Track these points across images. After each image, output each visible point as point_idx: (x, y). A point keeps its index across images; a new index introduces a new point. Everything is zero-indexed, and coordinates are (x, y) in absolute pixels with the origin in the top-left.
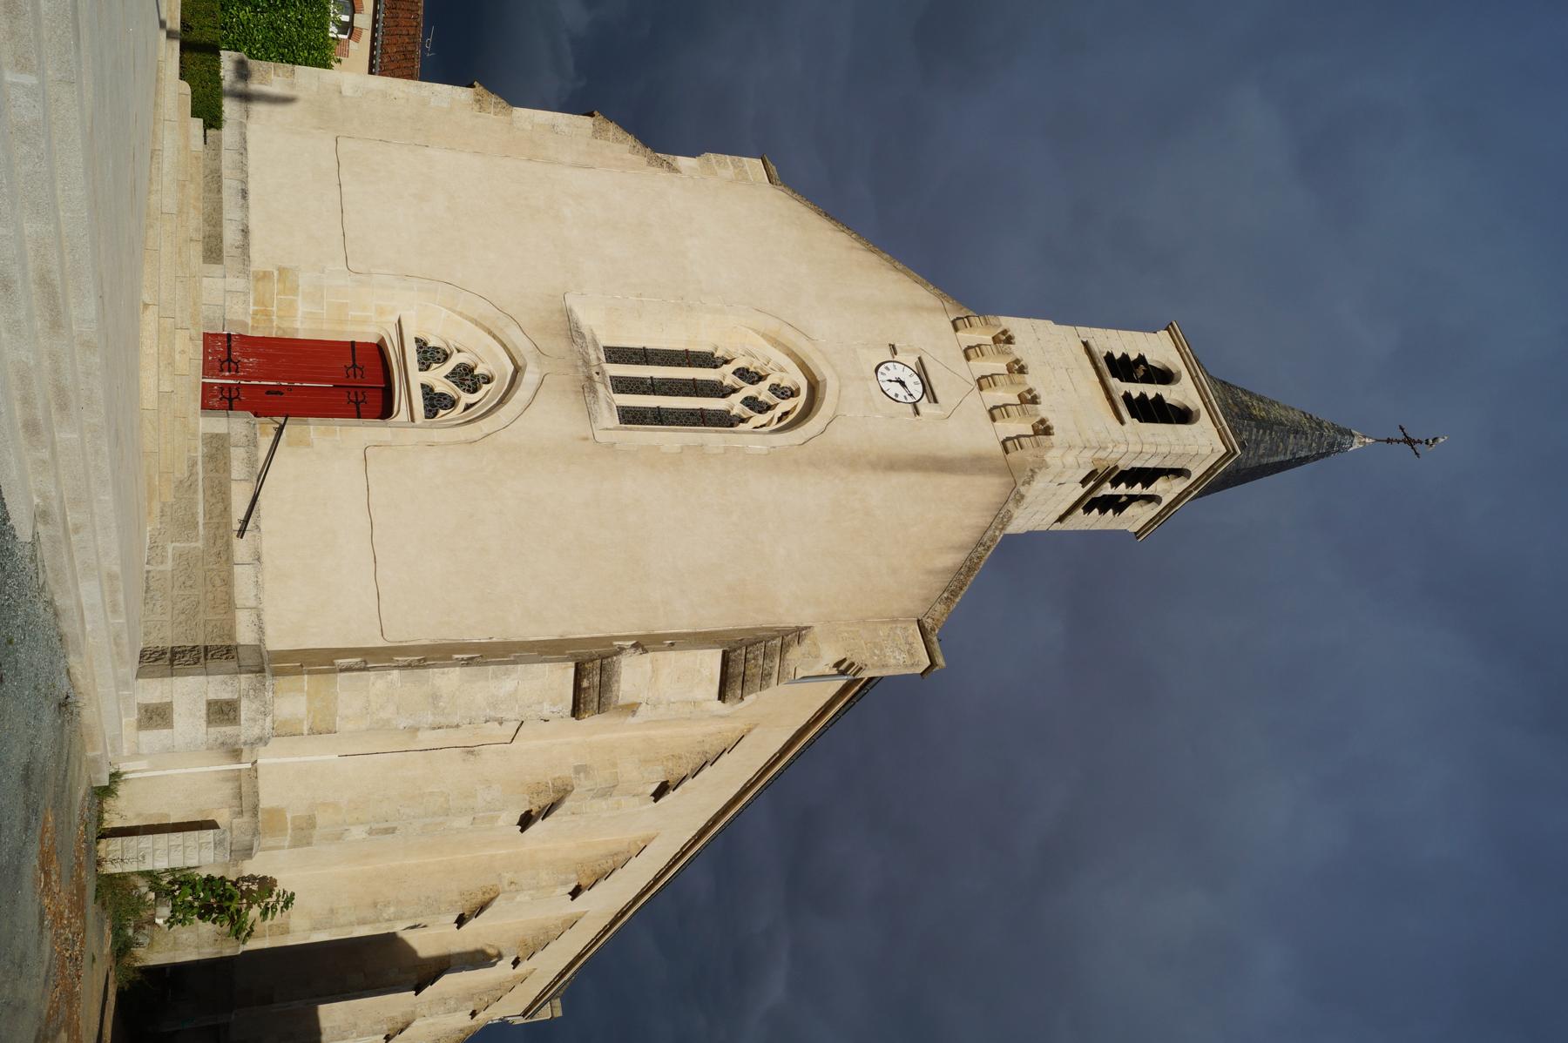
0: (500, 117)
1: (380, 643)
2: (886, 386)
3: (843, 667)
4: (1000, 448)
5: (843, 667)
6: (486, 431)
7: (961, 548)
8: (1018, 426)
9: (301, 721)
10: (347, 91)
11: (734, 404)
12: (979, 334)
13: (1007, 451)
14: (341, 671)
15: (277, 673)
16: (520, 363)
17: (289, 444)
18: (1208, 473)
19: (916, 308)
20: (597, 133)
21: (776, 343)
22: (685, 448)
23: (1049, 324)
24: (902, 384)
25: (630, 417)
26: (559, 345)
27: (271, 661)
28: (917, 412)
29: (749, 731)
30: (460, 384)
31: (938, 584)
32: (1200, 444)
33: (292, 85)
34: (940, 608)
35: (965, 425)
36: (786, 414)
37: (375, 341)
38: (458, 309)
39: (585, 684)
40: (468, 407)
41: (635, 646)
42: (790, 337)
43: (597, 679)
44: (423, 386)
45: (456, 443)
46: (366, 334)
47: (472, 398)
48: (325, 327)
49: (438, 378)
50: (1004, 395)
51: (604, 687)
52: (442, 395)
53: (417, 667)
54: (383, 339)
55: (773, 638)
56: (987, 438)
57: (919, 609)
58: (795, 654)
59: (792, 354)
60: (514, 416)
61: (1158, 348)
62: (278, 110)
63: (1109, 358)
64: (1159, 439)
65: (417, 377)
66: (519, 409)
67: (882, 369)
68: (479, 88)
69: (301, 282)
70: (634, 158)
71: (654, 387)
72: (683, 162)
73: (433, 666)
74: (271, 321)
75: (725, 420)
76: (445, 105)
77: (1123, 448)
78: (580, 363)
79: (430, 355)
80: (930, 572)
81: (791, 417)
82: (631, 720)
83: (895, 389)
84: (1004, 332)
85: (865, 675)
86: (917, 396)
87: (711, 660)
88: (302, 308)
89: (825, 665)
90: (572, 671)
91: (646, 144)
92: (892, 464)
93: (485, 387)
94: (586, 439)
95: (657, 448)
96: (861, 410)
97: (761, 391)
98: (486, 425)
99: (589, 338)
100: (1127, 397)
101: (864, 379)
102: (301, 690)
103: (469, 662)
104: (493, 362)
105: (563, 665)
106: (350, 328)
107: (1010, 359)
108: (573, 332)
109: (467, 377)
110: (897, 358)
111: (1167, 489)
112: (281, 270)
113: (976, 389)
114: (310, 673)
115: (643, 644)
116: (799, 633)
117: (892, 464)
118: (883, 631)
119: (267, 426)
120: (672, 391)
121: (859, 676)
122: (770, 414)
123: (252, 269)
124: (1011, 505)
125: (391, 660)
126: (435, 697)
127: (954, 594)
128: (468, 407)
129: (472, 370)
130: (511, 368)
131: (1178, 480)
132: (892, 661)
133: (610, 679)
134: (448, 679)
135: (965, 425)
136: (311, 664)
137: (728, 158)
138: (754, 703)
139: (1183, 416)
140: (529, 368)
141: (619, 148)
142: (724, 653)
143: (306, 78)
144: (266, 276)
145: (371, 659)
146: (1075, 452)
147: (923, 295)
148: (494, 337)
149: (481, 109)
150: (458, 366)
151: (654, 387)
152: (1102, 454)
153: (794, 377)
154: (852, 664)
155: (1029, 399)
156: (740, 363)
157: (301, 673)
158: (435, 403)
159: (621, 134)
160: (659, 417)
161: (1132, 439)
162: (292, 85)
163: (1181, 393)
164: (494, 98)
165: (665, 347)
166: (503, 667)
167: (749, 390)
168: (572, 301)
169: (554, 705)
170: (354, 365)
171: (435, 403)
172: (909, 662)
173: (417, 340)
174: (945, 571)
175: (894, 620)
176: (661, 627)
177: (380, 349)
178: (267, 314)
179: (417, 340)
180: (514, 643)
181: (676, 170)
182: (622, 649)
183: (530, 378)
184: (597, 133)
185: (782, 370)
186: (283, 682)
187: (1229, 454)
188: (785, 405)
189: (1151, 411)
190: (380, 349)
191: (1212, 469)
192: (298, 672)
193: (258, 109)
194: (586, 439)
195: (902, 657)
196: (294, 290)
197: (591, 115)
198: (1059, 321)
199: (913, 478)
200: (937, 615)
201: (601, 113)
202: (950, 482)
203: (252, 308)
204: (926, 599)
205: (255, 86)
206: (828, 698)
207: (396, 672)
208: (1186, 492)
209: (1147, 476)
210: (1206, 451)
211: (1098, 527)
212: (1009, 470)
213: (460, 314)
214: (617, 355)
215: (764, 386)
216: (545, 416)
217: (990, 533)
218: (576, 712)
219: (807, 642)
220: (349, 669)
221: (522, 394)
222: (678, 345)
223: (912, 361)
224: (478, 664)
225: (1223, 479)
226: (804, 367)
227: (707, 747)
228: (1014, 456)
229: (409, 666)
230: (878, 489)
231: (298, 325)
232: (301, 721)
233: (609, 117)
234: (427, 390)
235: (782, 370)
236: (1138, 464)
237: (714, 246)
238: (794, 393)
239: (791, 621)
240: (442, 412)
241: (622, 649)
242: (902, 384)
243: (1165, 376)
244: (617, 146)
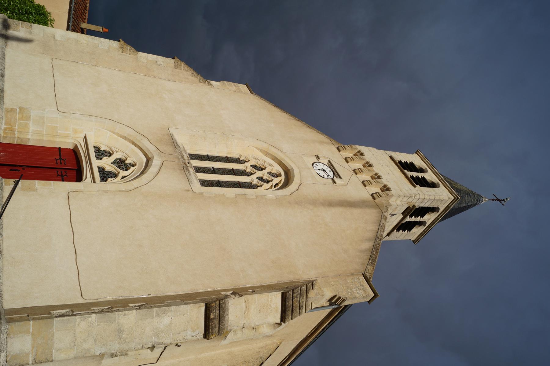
0: (132, 56)
1: (80, 301)
2: (319, 172)
3: (333, 301)
4: (371, 197)
5: (333, 301)
6: (136, 186)
7: (369, 240)
8: (375, 189)
9: (28, 354)
10: (58, 37)
11: (253, 180)
12: (348, 153)
13: (374, 198)
14: (56, 317)
15: (9, 321)
16: (150, 156)
17: (22, 190)
18: (445, 209)
19: (321, 143)
20: (176, 66)
21: (267, 154)
22: (237, 195)
23: (374, 149)
24: (324, 170)
25: (205, 183)
26: (169, 149)
27: (6, 314)
28: (334, 182)
29: (281, 343)
30: (119, 167)
31: (365, 257)
32: (442, 196)
33: (30, 33)
34: (370, 268)
35: (353, 188)
36: (277, 184)
37: (71, 147)
38: (116, 131)
39: (212, 316)
40: (123, 177)
41: (232, 294)
42: (273, 151)
43: (217, 313)
44: (99, 167)
45: (120, 191)
46: (67, 143)
47: (125, 173)
48: (44, 138)
49: (107, 163)
50: (365, 176)
51: (221, 318)
52: (109, 172)
53: (108, 312)
54: (76, 146)
55: (303, 286)
56: (365, 193)
57: (362, 270)
58: (312, 294)
59: (275, 159)
60: (149, 179)
61: (417, 161)
62: (22, 46)
63: (400, 162)
64: (430, 193)
65: (96, 163)
66: (152, 176)
67: (314, 165)
68: (122, 42)
69: (32, 114)
70: (193, 78)
71: (215, 171)
72: (213, 83)
73: (118, 310)
74: (14, 134)
75: (249, 186)
76: (106, 48)
77: (418, 197)
78: (180, 157)
79: (101, 154)
80: (361, 251)
81: (280, 185)
82: (224, 342)
83: (322, 173)
84: (359, 152)
85: (344, 304)
86: (332, 176)
87: (276, 298)
88: (32, 128)
89: (324, 302)
90: (203, 309)
91: (198, 73)
92: (330, 204)
93: (132, 168)
94: (188, 191)
95: (224, 195)
96: (310, 179)
97: (264, 174)
98: (136, 183)
99: (182, 148)
100: (412, 177)
101: (308, 168)
102: (28, 332)
103: (140, 307)
104: (135, 156)
105: (198, 305)
106: (58, 140)
107: (364, 162)
108: (175, 144)
109: (121, 164)
110: (320, 161)
111: (429, 218)
112: (21, 109)
113: (354, 174)
114: (33, 319)
115: (238, 292)
116: (311, 284)
117: (330, 204)
118: (349, 280)
119: (12, 182)
120: (222, 173)
121: (341, 305)
122: (270, 184)
123: (4, 107)
124: (383, 221)
125: (89, 309)
126: (120, 331)
127: (374, 261)
128: (123, 177)
129: (124, 161)
130: (145, 160)
131: (433, 214)
132: (357, 295)
133: (224, 313)
134: (128, 319)
135: (353, 188)
136: (35, 314)
137: (232, 83)
138: (291, 323)
139: (433, 185)
140: (155, 158)
141: (186, 74)
142: (283, 294)
143: (37, 30)
144: (12, 110)
145: (74, 310)
146: (400, 199)
147: (322, 137)
148: (136, 145)
149: (123, 51)
150: (117, 159)
151: (215, 171)
152: (410, 200)
153: (277, 169)
154: (340, 298)
155: (377, 177)
156: (253, 162)
157: (29, 320)
158: (105, 175)
159: (187, 67)
160: (219, 184)
161: (420, 193)
162: (30, 33)
163: (430, 176)
164: (129, 47)
165: (203, 174)
166: (162, 309)
167: (259, 174)
168: (172, 131)
169: (193, 331)
170: (60, 159)
171: (105, 175)
172: (365, 295)
173: (94, 147)
174: (367, 250)
175: (352, 274)
176: (243, 284)
177: (75, 152)
178: (13, 131)
179: (94, 147)
180: (163, 297)
181: (211, 85)
182: (227, 296)
183: (156, 162)
184: (176, 66)
185: (271, 165)
186: (14, 327)
187: (455, 199)
188: (276, 180)
189: (423, 183)
190: (75, 152)
191: (448, 207)
192: (27, 319)
193: (12, 44)
194: (188, 191)
195: (361, 293)
196: (28, 118)
197: (174, 58)
198: (378, 148)
199: (341, 209)
200: (370, 271)
201: (178, 58)
202: (357, 212)
203: (3, 126)
204: (363, 264)
205: (11, 32)
206: (320, 320)
207: (94, 316)
208: (436, 219)
209: (422, 211)
210: (447, 198)
211: (400, 239)
212: (378, 206)
213: (117, 134)
214: (194, 157)
215: (265, 172)
216: (166, 180)
217: (379, 233)
218: (207, 335)
219: (316, 288)
220: (62, 316)
221: (153, 170)
222: (224, 155)
223: (326, 162)
224: (146, 308)
225: (451, 212)
226: (281, 164)
227: (262, 355)
228: (378, 200)
229: (102, 311)
230: (329, 215)
231: (30, 137)
232: (28, 354)
233: (181, 59)
234: (101, 170)
235: (271, 165)
236: (422, 205)
237: (233, 118)
238: (280, 175)
239: (306, 276)
240: (110, 179)
241: (227, 296)
242: (324, 170)
243: (422, 171)
244: (185, 73)
